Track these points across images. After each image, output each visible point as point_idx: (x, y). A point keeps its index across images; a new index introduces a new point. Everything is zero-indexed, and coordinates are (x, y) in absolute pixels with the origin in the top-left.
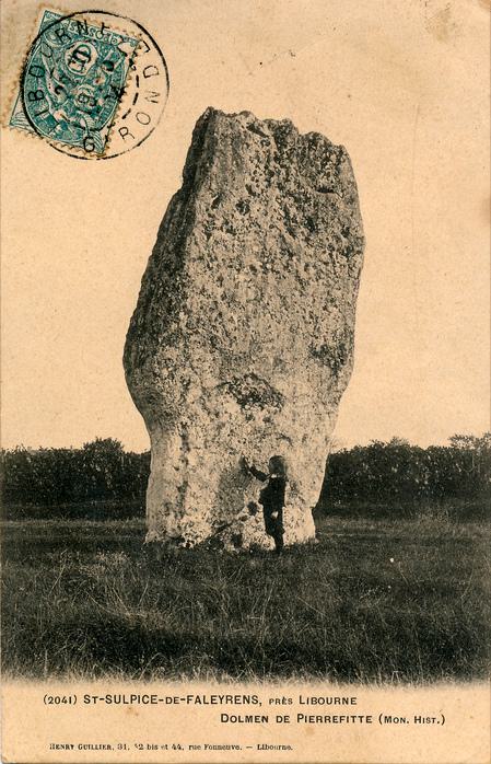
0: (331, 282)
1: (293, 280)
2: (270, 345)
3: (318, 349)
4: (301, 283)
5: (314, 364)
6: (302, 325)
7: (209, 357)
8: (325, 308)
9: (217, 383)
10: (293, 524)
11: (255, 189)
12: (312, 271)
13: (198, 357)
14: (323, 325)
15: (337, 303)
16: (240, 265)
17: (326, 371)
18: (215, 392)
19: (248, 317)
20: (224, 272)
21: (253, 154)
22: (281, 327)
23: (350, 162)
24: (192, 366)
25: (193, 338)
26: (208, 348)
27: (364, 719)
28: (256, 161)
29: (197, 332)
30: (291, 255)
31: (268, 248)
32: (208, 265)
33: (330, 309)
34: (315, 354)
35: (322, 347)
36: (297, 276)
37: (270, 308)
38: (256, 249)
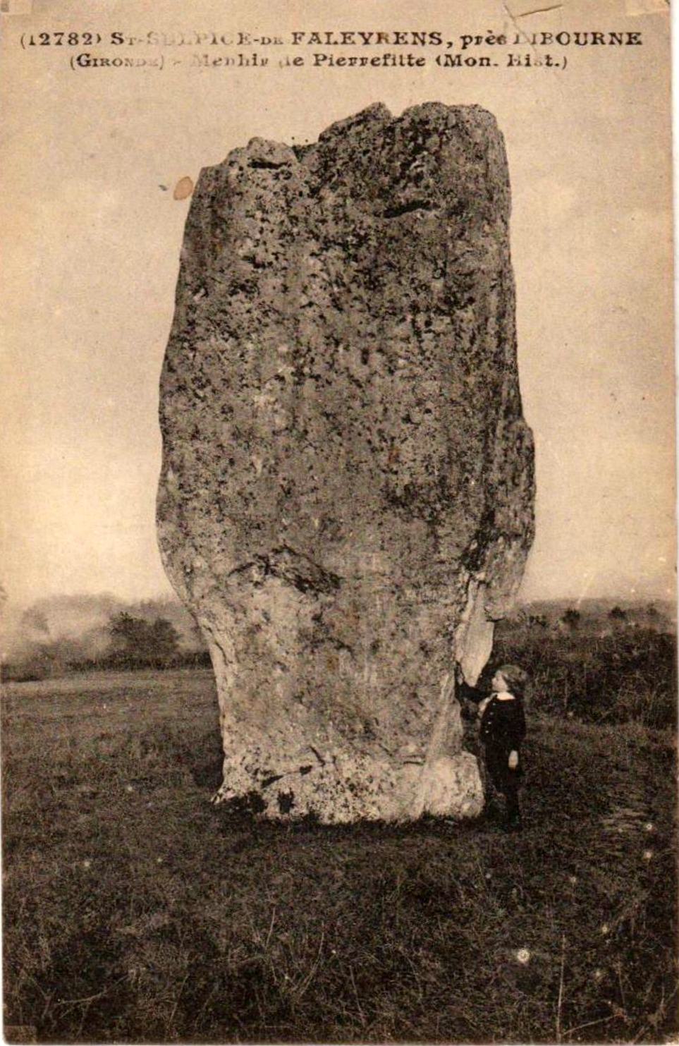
0: (419, 370)
1: (346, 383)
2: (312, 497)
3: (399, 492)
4: (360, 386)
5: (395, 523)
6: (365, 454)
7: (217, 528)
8: (407, 419)
9: (232, 567)
10: (374, 787)
11: (261, 256)
12: (377, 360)
13: (200, 531)
14: (406, 451)
15: (430, 405)
16: (260, 380)
17: (418, 527)
18: (234, 580)
19: (277, 458)
20: (230, 397)
21: (251, 204)
22: (329, 466)
23: (462, 106)
24: (194, 546)
25: (191, 504)
26: (215, 514)
27: (266, 41)
28: (259, 214)
29: (197, 496)
30: (337, 343)
31: (303, 340)
32: (196, 396)
33: (416, 417)
34: (395, 501)
35: (406, 488)
36: (350, 376)
37: (310, 436)
38: (284, 349)
